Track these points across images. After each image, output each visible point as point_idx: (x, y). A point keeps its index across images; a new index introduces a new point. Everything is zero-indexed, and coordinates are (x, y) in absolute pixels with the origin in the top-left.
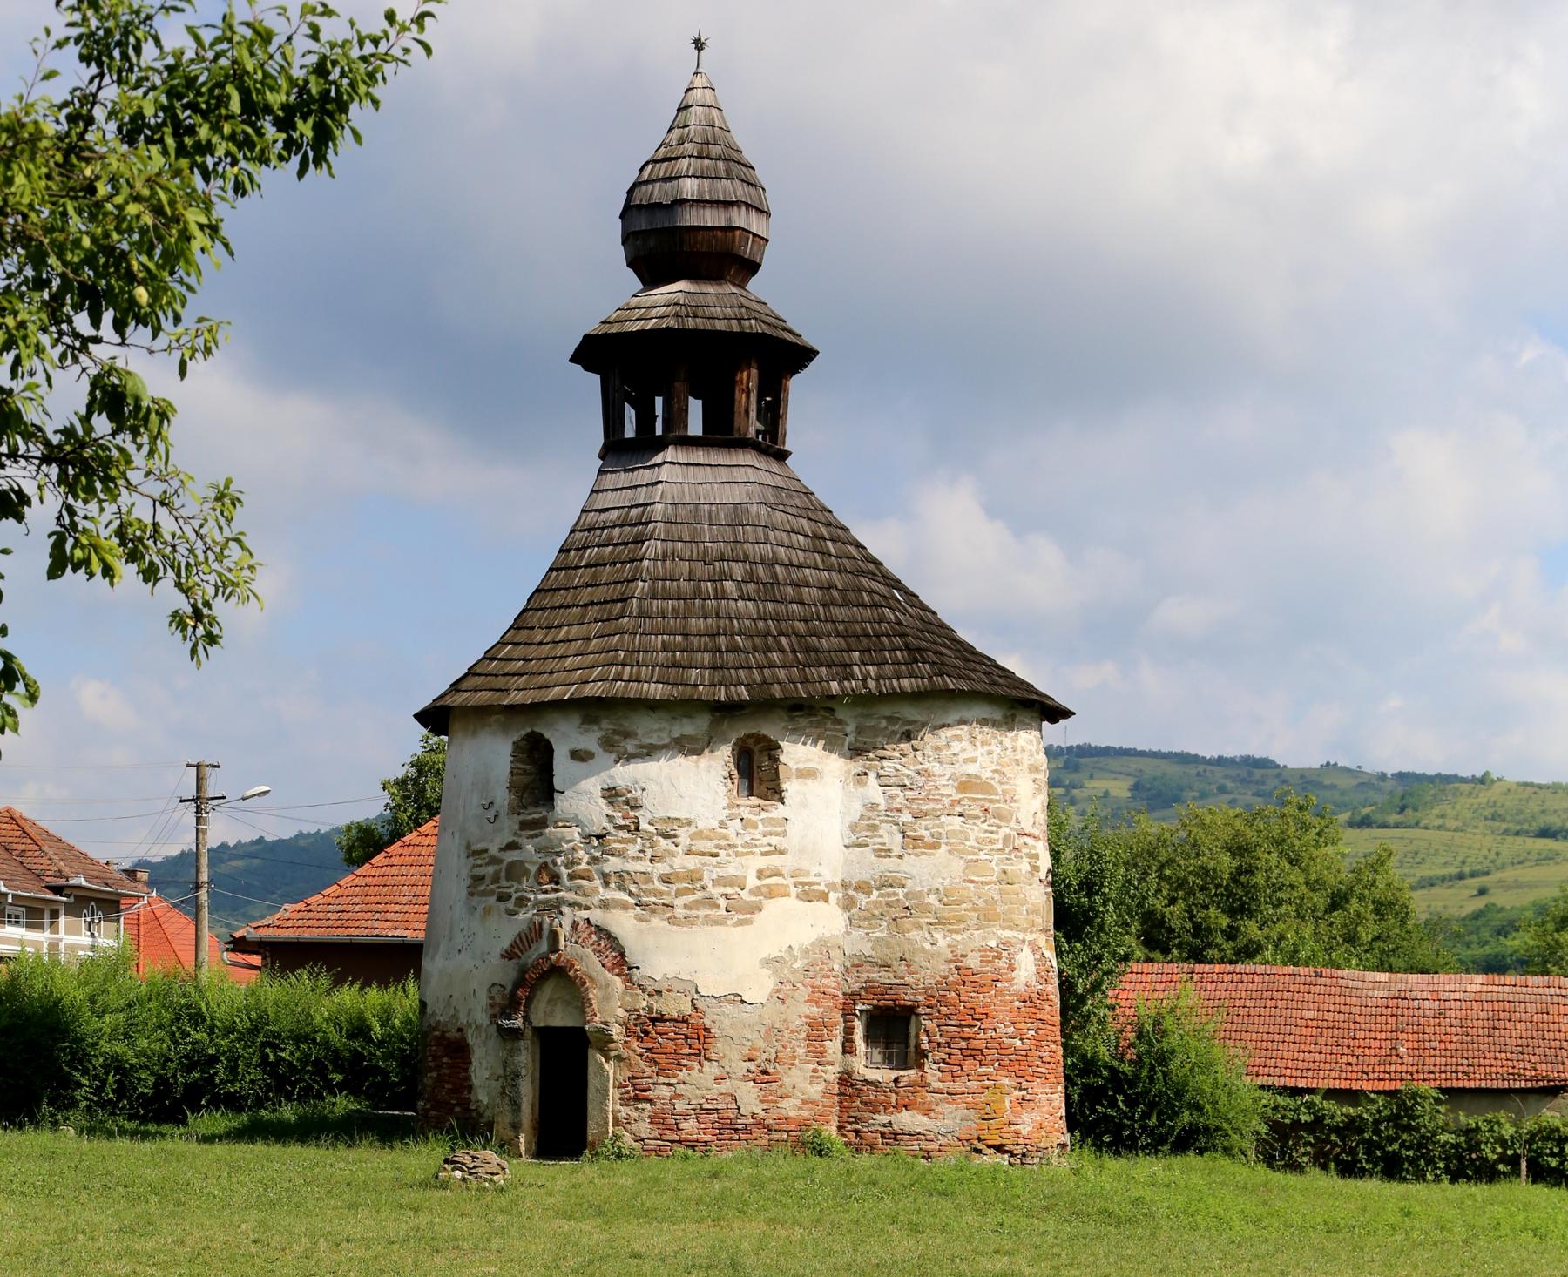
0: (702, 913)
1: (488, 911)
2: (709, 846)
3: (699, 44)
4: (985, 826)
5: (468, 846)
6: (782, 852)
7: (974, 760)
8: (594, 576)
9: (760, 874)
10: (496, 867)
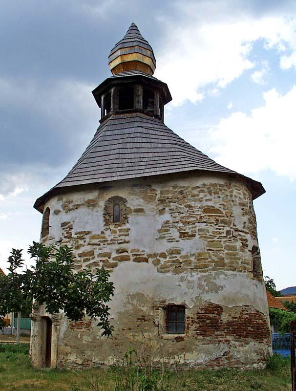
4: (217, 227)
6: (127, 243)
7: (210, 200)
9: (118, 251)
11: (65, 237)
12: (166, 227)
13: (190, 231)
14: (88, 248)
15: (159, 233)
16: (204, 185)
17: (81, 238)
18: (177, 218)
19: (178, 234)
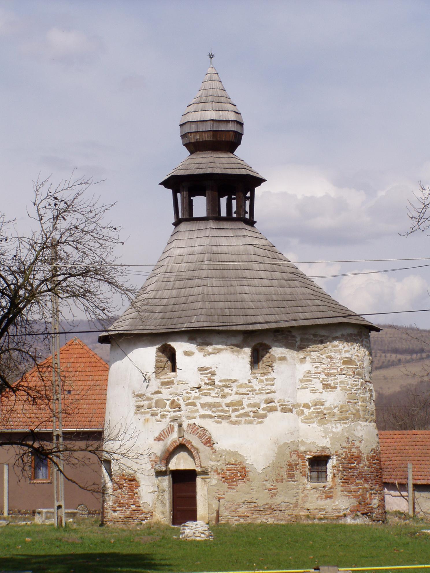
0: (243, 419)
1: (147, 420)
2: (244, 390)
3: (211, 56)
4: (354, 379)
5: (134, 393)
6: (274, 392)
10: (150, 402)
11: (206, 384)
12: (308, 377)
13: (332, 383)
14: (237, 398)
15: (301, 382)
17: (227, 386)
18: (319, 369)
19: (321, 386)
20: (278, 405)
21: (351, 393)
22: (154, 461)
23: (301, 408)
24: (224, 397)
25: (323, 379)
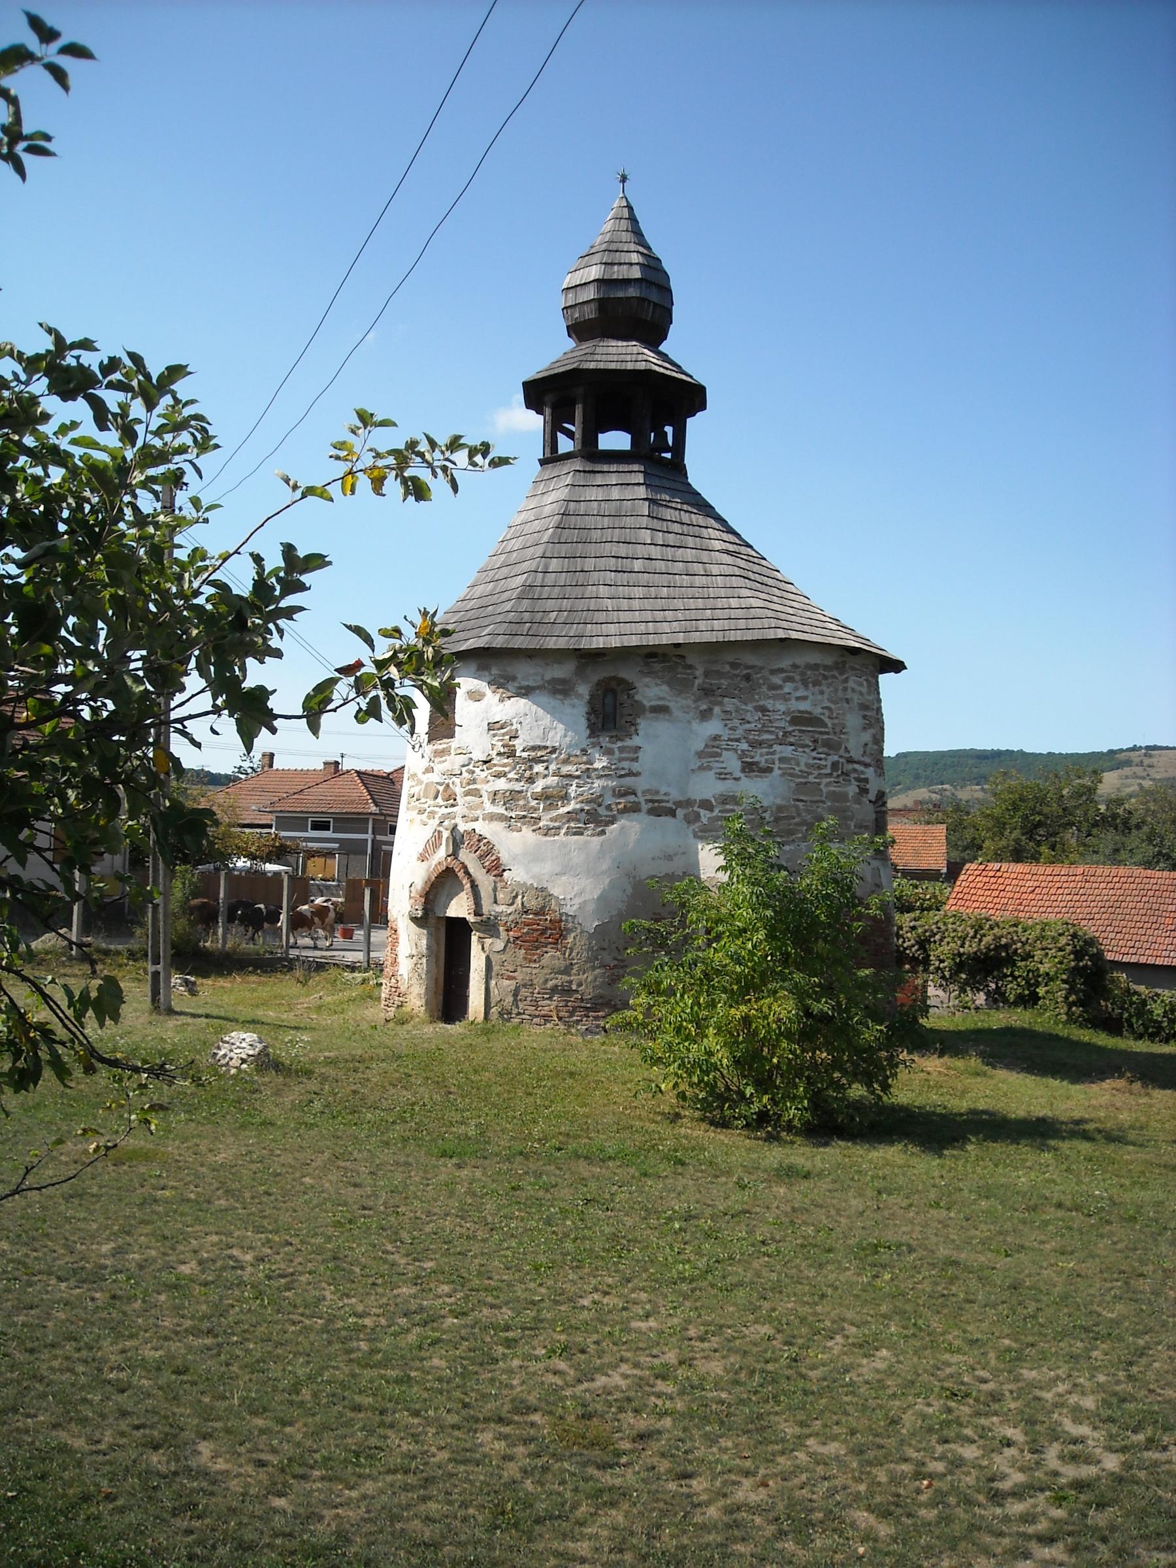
3: (624, 179)
4: (814, 754)
7: (805, 698)
8: (546, 566)
11: (499, 754)
13: (763, 760)
15: (700, 757)
16: (795, 666)
17: (538, 760)
20: (642, 799)
21: (806, 783)
22: (997, 819)
23: (696, 809)
24: (531, 780)
25: (743, 751)
